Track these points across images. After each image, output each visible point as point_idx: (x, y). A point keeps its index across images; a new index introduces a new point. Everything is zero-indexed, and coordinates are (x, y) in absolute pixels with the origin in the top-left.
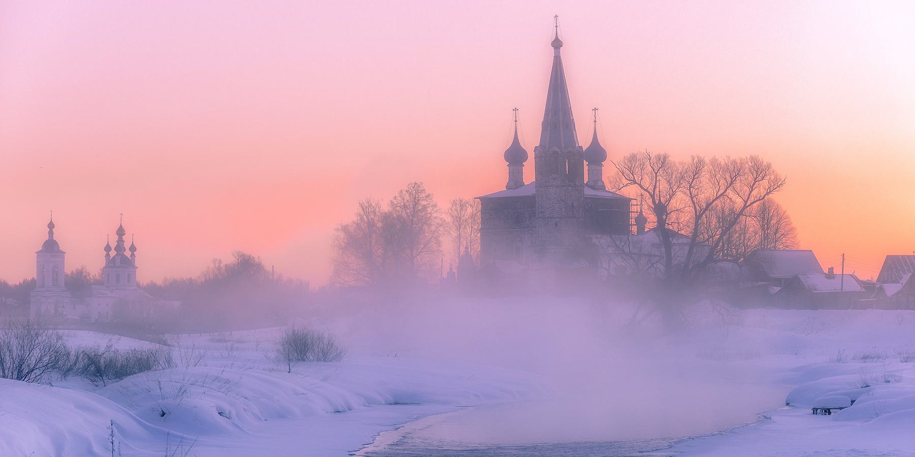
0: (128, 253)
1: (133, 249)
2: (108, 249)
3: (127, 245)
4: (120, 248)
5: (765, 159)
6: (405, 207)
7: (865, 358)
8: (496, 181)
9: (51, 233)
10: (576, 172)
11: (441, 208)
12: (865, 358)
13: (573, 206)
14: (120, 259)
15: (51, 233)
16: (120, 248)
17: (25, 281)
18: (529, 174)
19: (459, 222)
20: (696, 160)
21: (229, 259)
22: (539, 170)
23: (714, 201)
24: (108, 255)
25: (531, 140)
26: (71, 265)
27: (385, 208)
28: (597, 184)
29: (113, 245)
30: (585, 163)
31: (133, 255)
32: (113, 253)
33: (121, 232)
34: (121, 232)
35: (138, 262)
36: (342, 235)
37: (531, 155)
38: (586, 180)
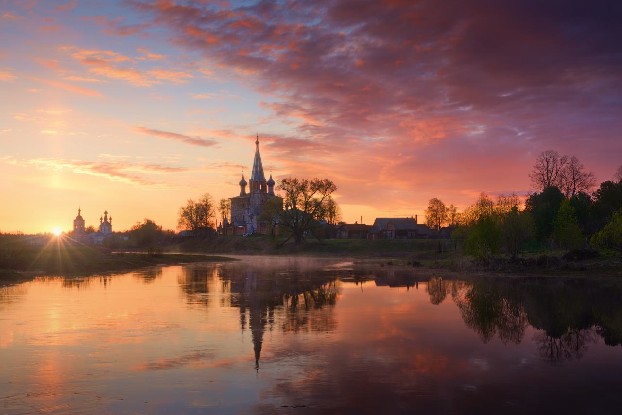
0: (109, 220)
1: (111, 219)
2: (101, 219)
3: (108, 218)
4: (106, 218)
5: (330, 180)
6: (204, 201)
7: (86, 313)
8: (236, 192)
9: (79, 213)
10: (264, 188)
11: (216, 204)
12: (86, 313)
13: (263, 201)
14: (106, 224)
15: (79, 213)
16: (106, 218)
17: (37, 235)
18: (248, 190)
19: (223, 207)
20: (304, 181)
21: (143, 222)
22: (251, 188)
23: (322, 199)
24: (101, 221)
25: (249, 176)
26: (87, 225)
27: (197, 202)
28: (271, 194)
29: (103, 217)
30: (267, 186)
31: (111, 221)
32: (103, 220)
33: (106, 213)
34: (106, 213)
35: (113, 224)
36: (182, 211)
37: (248, 182)
38: (267, 192)
